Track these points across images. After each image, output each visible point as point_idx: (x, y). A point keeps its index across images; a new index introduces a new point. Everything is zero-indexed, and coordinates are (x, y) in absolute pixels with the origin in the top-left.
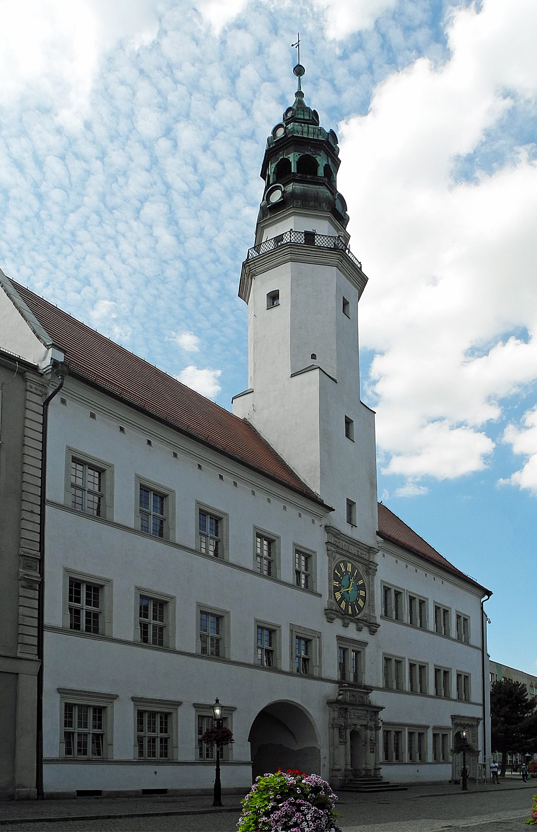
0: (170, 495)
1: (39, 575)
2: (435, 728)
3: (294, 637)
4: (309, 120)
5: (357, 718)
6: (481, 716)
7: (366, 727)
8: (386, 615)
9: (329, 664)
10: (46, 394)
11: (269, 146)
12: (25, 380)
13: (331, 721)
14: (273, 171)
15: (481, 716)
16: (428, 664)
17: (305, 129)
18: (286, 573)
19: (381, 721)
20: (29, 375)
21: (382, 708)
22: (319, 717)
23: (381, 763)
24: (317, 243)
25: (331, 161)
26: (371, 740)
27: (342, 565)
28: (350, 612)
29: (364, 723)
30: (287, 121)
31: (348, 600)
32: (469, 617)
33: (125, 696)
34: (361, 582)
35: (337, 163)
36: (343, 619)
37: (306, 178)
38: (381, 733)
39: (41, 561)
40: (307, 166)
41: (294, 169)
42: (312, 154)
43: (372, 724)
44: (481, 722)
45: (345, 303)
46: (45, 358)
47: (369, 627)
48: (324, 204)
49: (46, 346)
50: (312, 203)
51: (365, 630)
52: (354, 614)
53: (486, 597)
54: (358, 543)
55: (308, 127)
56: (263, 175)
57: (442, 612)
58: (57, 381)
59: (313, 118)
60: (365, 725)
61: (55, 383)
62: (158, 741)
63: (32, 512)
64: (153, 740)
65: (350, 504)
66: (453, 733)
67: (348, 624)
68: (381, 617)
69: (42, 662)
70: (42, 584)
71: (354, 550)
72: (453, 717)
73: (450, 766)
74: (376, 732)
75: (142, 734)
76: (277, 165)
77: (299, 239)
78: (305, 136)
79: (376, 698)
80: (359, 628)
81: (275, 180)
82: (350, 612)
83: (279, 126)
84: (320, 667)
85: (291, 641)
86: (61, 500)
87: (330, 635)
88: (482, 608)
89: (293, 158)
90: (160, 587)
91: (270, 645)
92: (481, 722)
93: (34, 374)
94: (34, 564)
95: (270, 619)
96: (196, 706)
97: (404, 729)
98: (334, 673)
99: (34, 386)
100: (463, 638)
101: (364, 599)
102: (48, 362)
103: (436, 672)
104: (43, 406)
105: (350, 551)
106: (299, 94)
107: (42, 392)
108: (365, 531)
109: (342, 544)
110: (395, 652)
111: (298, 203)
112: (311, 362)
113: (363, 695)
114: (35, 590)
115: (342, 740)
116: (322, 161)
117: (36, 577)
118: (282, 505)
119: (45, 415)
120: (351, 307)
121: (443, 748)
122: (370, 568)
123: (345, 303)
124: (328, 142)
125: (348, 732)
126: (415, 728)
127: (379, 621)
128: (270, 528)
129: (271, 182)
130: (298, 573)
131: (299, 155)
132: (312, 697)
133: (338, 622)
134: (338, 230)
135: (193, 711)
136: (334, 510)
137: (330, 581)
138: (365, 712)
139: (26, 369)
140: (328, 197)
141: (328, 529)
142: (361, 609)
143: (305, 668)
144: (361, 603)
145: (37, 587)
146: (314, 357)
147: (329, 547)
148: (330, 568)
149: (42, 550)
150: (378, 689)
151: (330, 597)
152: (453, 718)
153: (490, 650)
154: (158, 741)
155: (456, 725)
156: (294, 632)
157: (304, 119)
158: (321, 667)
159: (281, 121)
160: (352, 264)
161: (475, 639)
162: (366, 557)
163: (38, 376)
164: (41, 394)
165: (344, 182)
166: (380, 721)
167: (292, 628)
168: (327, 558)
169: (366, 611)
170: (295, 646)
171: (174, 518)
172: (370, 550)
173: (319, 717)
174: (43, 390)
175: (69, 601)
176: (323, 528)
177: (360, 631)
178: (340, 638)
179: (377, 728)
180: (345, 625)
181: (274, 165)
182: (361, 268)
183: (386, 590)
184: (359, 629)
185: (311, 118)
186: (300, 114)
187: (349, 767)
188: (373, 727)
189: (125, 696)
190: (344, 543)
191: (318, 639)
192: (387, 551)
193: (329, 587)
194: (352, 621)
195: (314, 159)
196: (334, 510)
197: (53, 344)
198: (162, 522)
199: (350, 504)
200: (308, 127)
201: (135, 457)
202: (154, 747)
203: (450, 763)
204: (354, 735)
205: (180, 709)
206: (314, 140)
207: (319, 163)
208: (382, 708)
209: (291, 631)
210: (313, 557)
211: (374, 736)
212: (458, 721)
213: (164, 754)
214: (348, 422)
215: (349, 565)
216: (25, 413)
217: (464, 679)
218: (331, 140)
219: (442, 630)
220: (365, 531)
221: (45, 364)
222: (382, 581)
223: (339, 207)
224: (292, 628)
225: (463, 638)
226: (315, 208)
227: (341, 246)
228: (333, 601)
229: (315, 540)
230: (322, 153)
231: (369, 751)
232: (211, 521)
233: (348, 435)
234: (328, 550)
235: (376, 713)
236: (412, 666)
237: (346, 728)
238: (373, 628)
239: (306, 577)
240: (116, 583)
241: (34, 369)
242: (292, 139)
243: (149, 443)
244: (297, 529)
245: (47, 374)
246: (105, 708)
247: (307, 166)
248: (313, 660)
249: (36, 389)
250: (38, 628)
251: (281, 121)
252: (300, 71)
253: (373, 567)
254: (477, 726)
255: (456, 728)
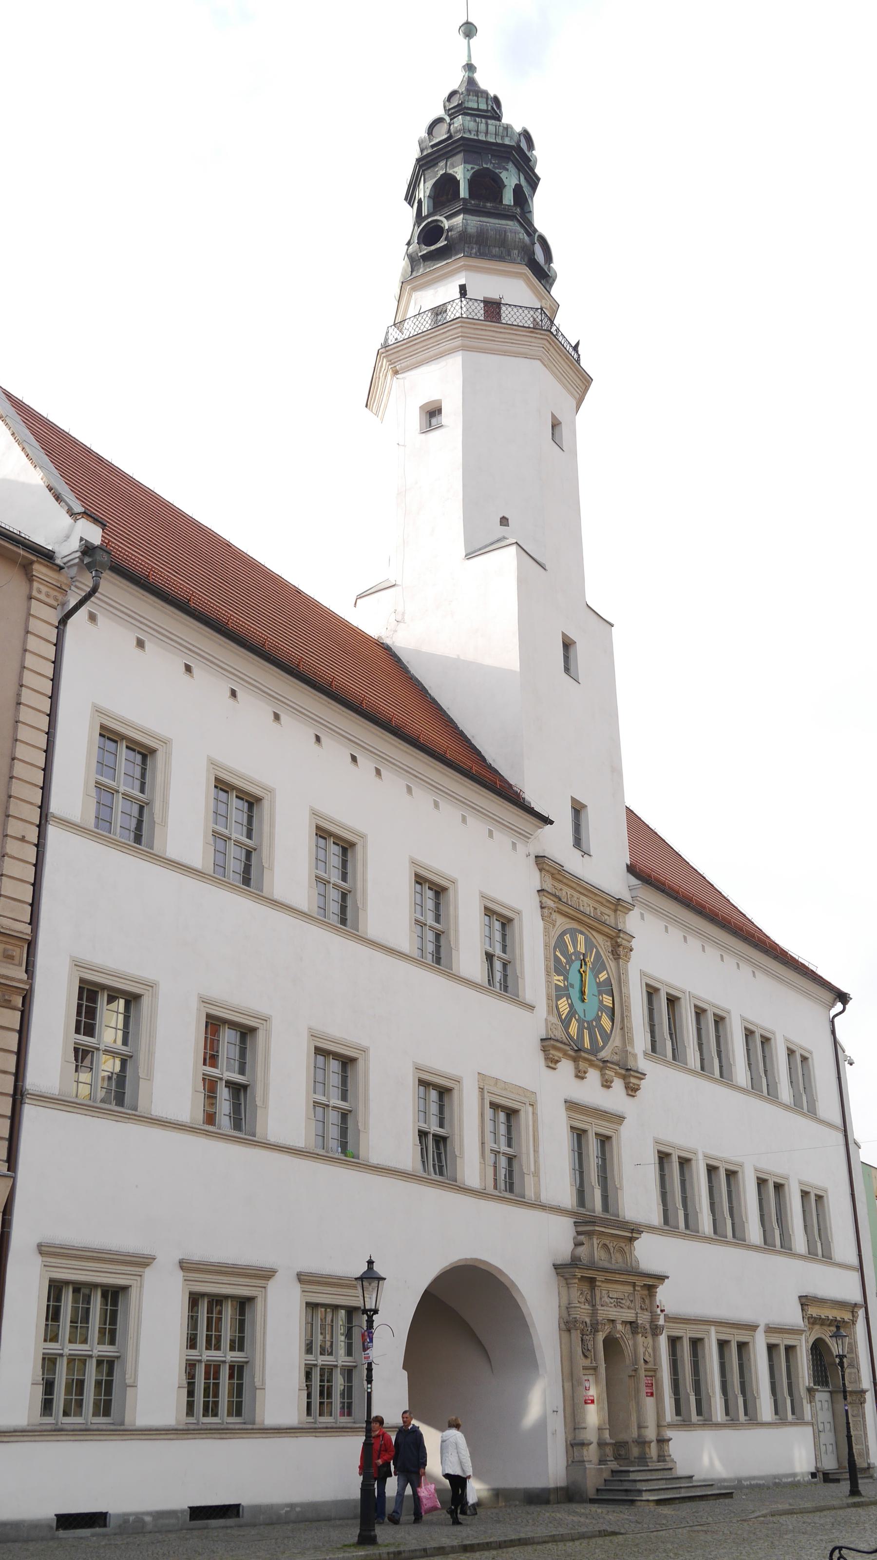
1: (24, 976)
2: (770, 1330)
3: (487, 1105)
4: (487, 111)
5: (615, 1308)
6: (858, 1298)
7: (633, 1325)
8: (654, 1049)
9: (553, 1170)
10: (63, 604)
11: (422, 151)
12: (30, 578)
13: (565, 1315)
14: (427, 194)
15: (858, 1298)
17: (482, 127)
18: (469, 958)
19: (662, 1311)
20: (40, 570)
21: (662, 1278)
22: (541, 1302)
23: (671, 1426)
24: (507, 319)
25: (525, 178)
26: (646, 1362)
27: (567, 938)
28: (587, 1044)
29: (629, 1316)
30: (453, 113)
31: (582, 1016)
32: (811, 1053)
33: (167, 1259)
34: (603, 976)
35: (534, 181)
36: (575, 1060)
37: (485, 207)
38: (663, 1341)
39: (31, 945)
40: (485, 187)
41: (463, 192)
42: (494, 167)
43: (644, 1319)
44: (861, 1313)
45: (555, 425)
46: (68, 537)
47: (624, 1077)
48: (516, 252)
49: (72, 513)
50: (495, 251)
51: (618, 1085)
52: (595, 1050)
53: (839, 1006)
54: (596, 891)
55: (487, 124)
56: (410, 197)
57: (758, 1042)
58: (87, 581)
59: (492, 109)
60: (631, 1323)
61: (83, 583)
62: (225, 1372)
63: (23, 839)
65: (578, 809)
66: (807, 1341)
67: (585, 1072)
68: (645, 1054)
69: (14, 1179)
70: (27, 998)
71: (587, 905)
72: (804, 1300)
73: (809, 1430)
74: (654, 1341)
76: (435, 185)
77: (521, 318)
78: (482, 137)
79: (650, 1253)
80: (607, 1081)
81: (431, 210)
82: (587, 1044)
83: (438, 121)
85: (482, 1115)
86: (76, 816)
87: (554, 1093)
88: (833, 1032)
89: (461, 172)
90: (241, 998)
91: (441, 1125)
92: (861, 1313)
93: (47, 566)
94: (18, 950)
95: (442, 1065)
97: (708, 1332)
98: (566, 1197)
99: (44, 589)
100: (804, 1103)
102: (74, 545)
103: (759, 1185)
104: (57, 627)
105: (582, 909)
106: (470, 67)
107: (56, 600)
108: (605, 867)
109: (566, 892)
110: (681, 1140)
111: (472, 248)
112: (502, 531)
113: (623, 1245)
114: (14, 1008)
115: (587, 1363)
116: (510, 178)
117: (20, 981)
119: (59, 645)
120: (565, 429)
121: (790, 1385)
122: (619, 945)
123: (555, 425)
124: (519, 149)
125: (601, 1337)
126: (729, 1330)
127: (643, 1064)
128: (441, 865)
129: (425, 212)
130: (489, 957)
131: (472, 168)
132: (526, 1248)
133: (566, 1067)
134: (540, 297)
135: (296, 1289)
136: (551, 822)
137: (548, 974)
138: (629, 1289)
139: (34, 558)
140: (522, 241)
141: (541, 861)
142: (607, 1037)
143: (509, 1182)
144: (606, 1022)
145: (18, 1001)
146: (504, 521)
147: (545, 899)
148: (546, 945)
149: (34, 920)
150: (652, 1229)
151: (550, 1011)
152: (805, 1301)
153: (858, 1132)
154: (225, 1372)
155: (813, 1321)
156: (486, 1093)
157: (478, 110)
158: (538, 1176)
159: (440, 112)
160: (565, 355)
161: (828, 1107)
162: (611, 920)
163: (54, 570)
164: (55, 604)
165: (546, 213)
166: (659, 1310)
167: (484, 1083)
169: (616, 1041)
170: (489, 1126)
171: (271, 845)
172: (618, 905)
173: (541, 1302)
174: (60, 597)
175: (76, 1033)
176: (532, 858)
177: (609, 1087)
178: (572, 1106)
179: (656, 1331)
180: (580, 1075)
181: (430, 184)
182: (578, 361)
183: (651, 992)
184: (607, 1084)
185: (490, 108)
186: (473, 103)
187: (606, 1435)
188: (648, 1326)
189: (167, 1259)
190: (570, 892)
191: (530, 1109)
192: (648, 906)
193: (548, 987)
194: (592, 1064)
196: (551, 822)
197: (84, 513)
198: (249, 854)
199: (578, 809)
200: (487, 124)
201: (209, 718)
203: (807, 1424)
204: (612, 1345)
205: (273, 1286)
206: (496, 144)
207: (506, 182)
208: (662, 1278)
209: (482, 1089)
210: (516, 922)
211: (650, 1350)
212: (813, 1311)
214: (568, 645)
215: (581, 938)
216: (25, 642)
217: (814, 1201)
218: (524, 145)
219: (762, 1086)
220: (605, 867)
221: (67, 549)
222: (643, 974)
223: (540, 256)
224: (484, 1083)
225: (804, 1103)
226: (501, 258)
227: (546, 323)
228: (555, 1020)
229: (520, 890)
230: (510, 166)
231: (644, 1390)
232: (339, 846)
233: (567, 670)
234: (542, 908)
235: (651, 1290)
236: (712, 1170)
237: (595, 1330)
238: (632, 1081)
239: (505, 966)
240: (164, 990)
241: (47, 556)
242: (461, 142)
243: (233, 693)
244: (488, 865)
245: (69, 567)
246: (125, 1289)
247: (485, 187)
248: (524, 1158)
249: (48, 595)
250: (14, 1096)
251: (440, 112)
252: (470, 31)
253: (624, 942)
254: (854, 1322)
255: (811, 1329)
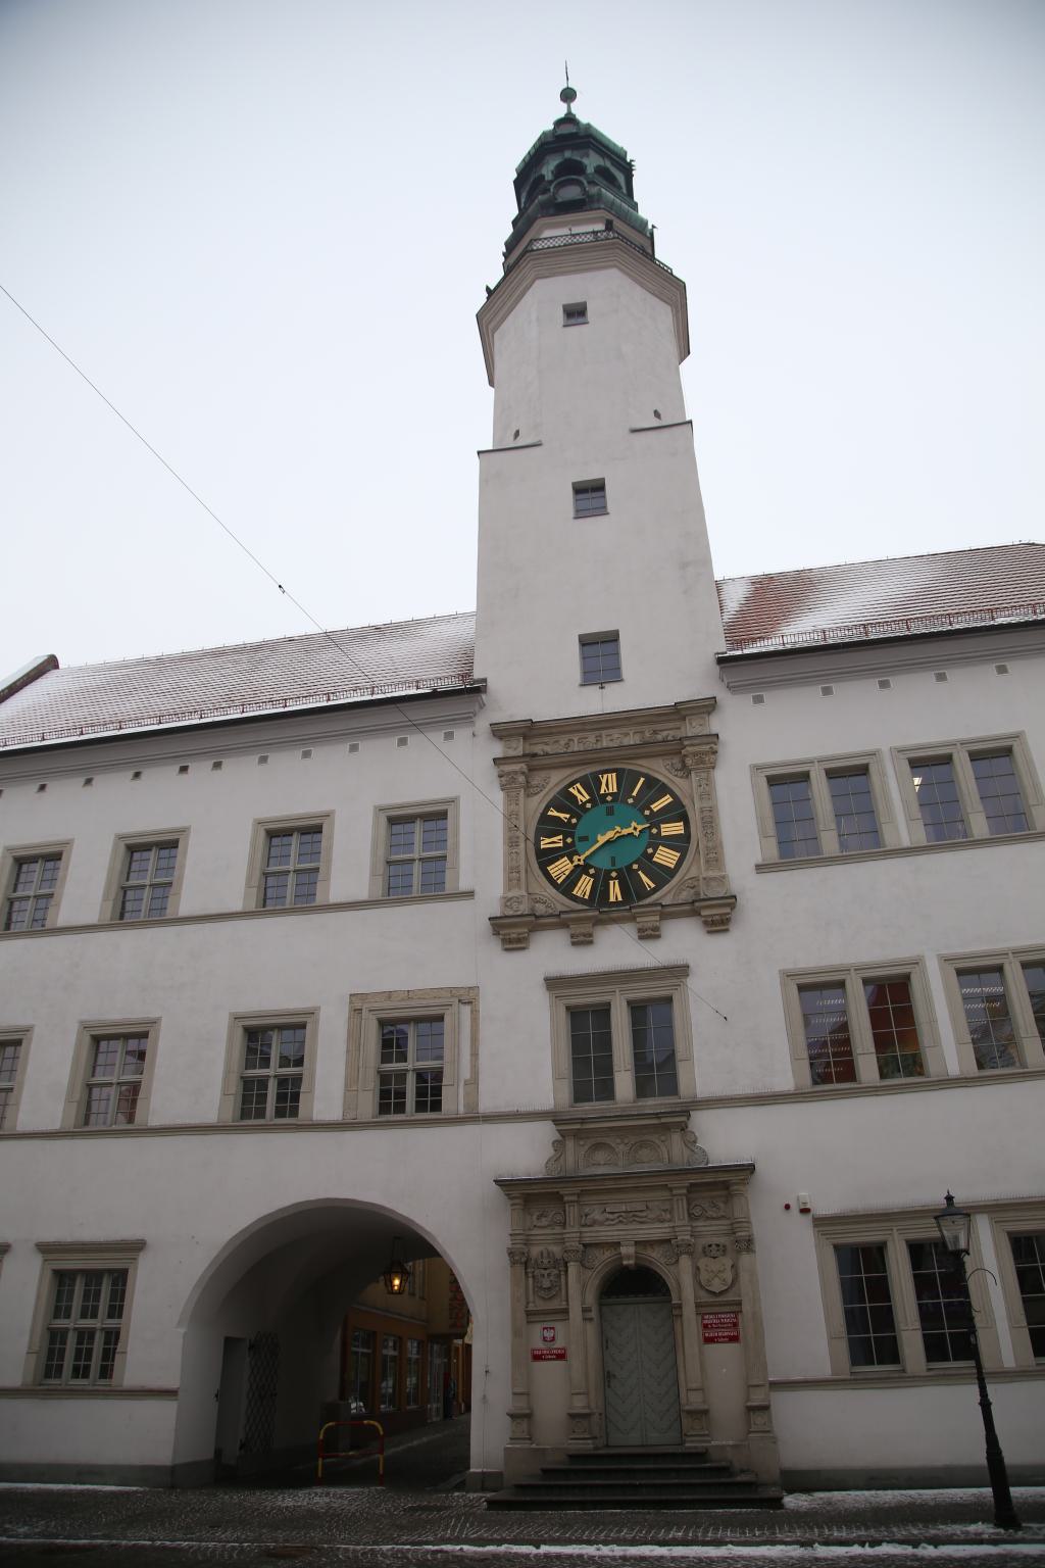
0: (813, 768)
16: (917, 962)
64: (85, 1336)
75: (61, 1323)
84: (474, 1081)
96: (45, 1249)
101: (680, 843)
118: (299, 753)
132: (441, 1184)
135: (37, 1261)
168: (499, 797)
195: (581, 163)
202: (78, 1353)
213: (106, 1372)
